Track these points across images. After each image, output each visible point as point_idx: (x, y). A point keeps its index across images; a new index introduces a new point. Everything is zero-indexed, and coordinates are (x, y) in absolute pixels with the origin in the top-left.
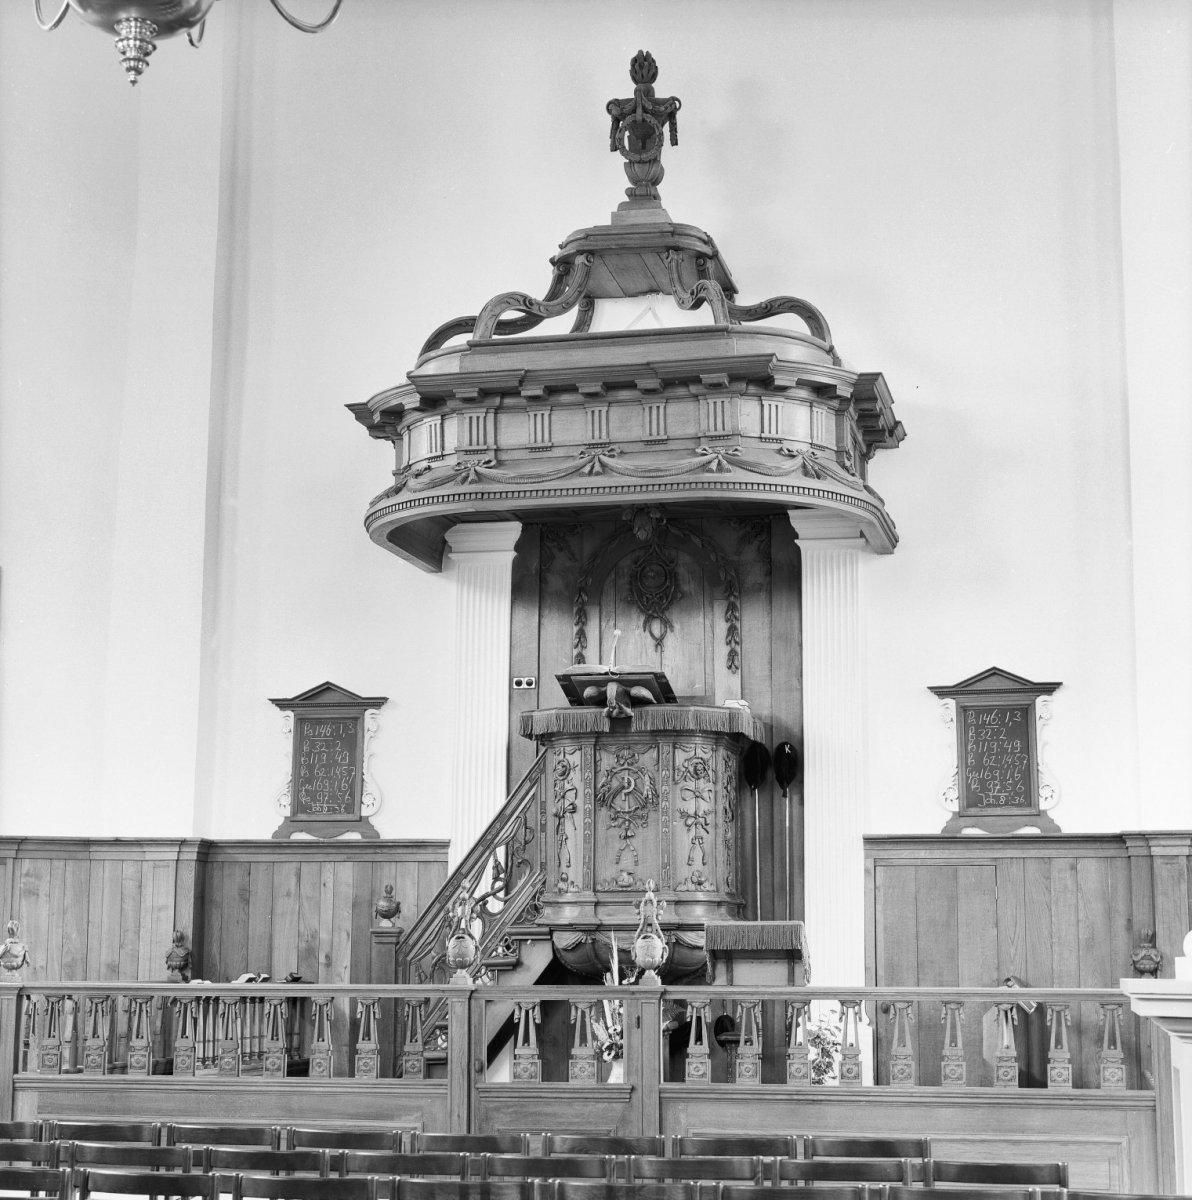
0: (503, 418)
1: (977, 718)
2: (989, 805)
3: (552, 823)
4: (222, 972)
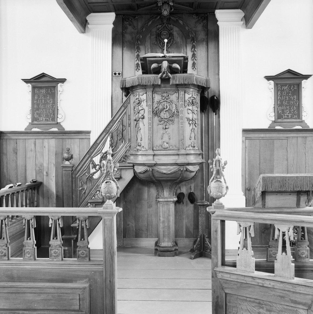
1: (281, 88)
2: (285, 118)
3: (133, 123)
4: (8, 178)
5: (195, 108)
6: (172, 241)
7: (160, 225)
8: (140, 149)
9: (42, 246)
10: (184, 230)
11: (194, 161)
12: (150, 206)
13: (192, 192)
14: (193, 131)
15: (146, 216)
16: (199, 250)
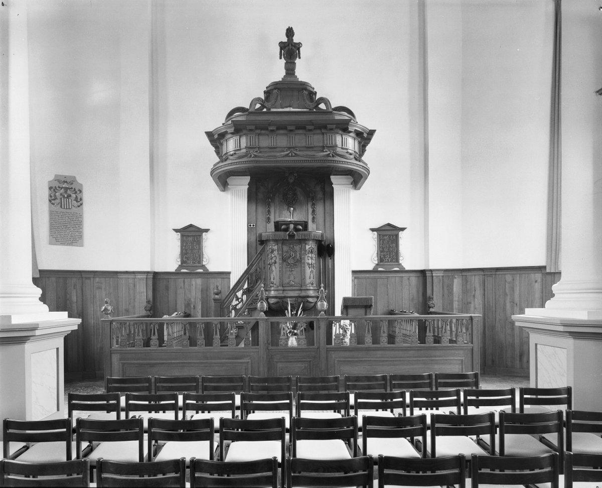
0: (261, 137)
11: (313, 295)
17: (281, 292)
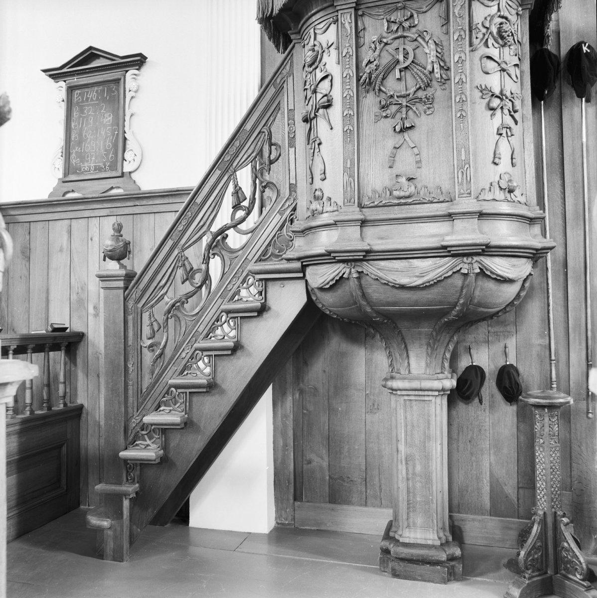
4: (9, 321)
5: (509, 56)
6: (440, 525)
7: (398, 470)
8: (320, 208)
9: (82, 507)
10: (486, 489)
12: (376, 407)
13: (512, 365)
14: (504, 135)
15: (363, 436)
16: (539, 570)
17: (354, 231)
